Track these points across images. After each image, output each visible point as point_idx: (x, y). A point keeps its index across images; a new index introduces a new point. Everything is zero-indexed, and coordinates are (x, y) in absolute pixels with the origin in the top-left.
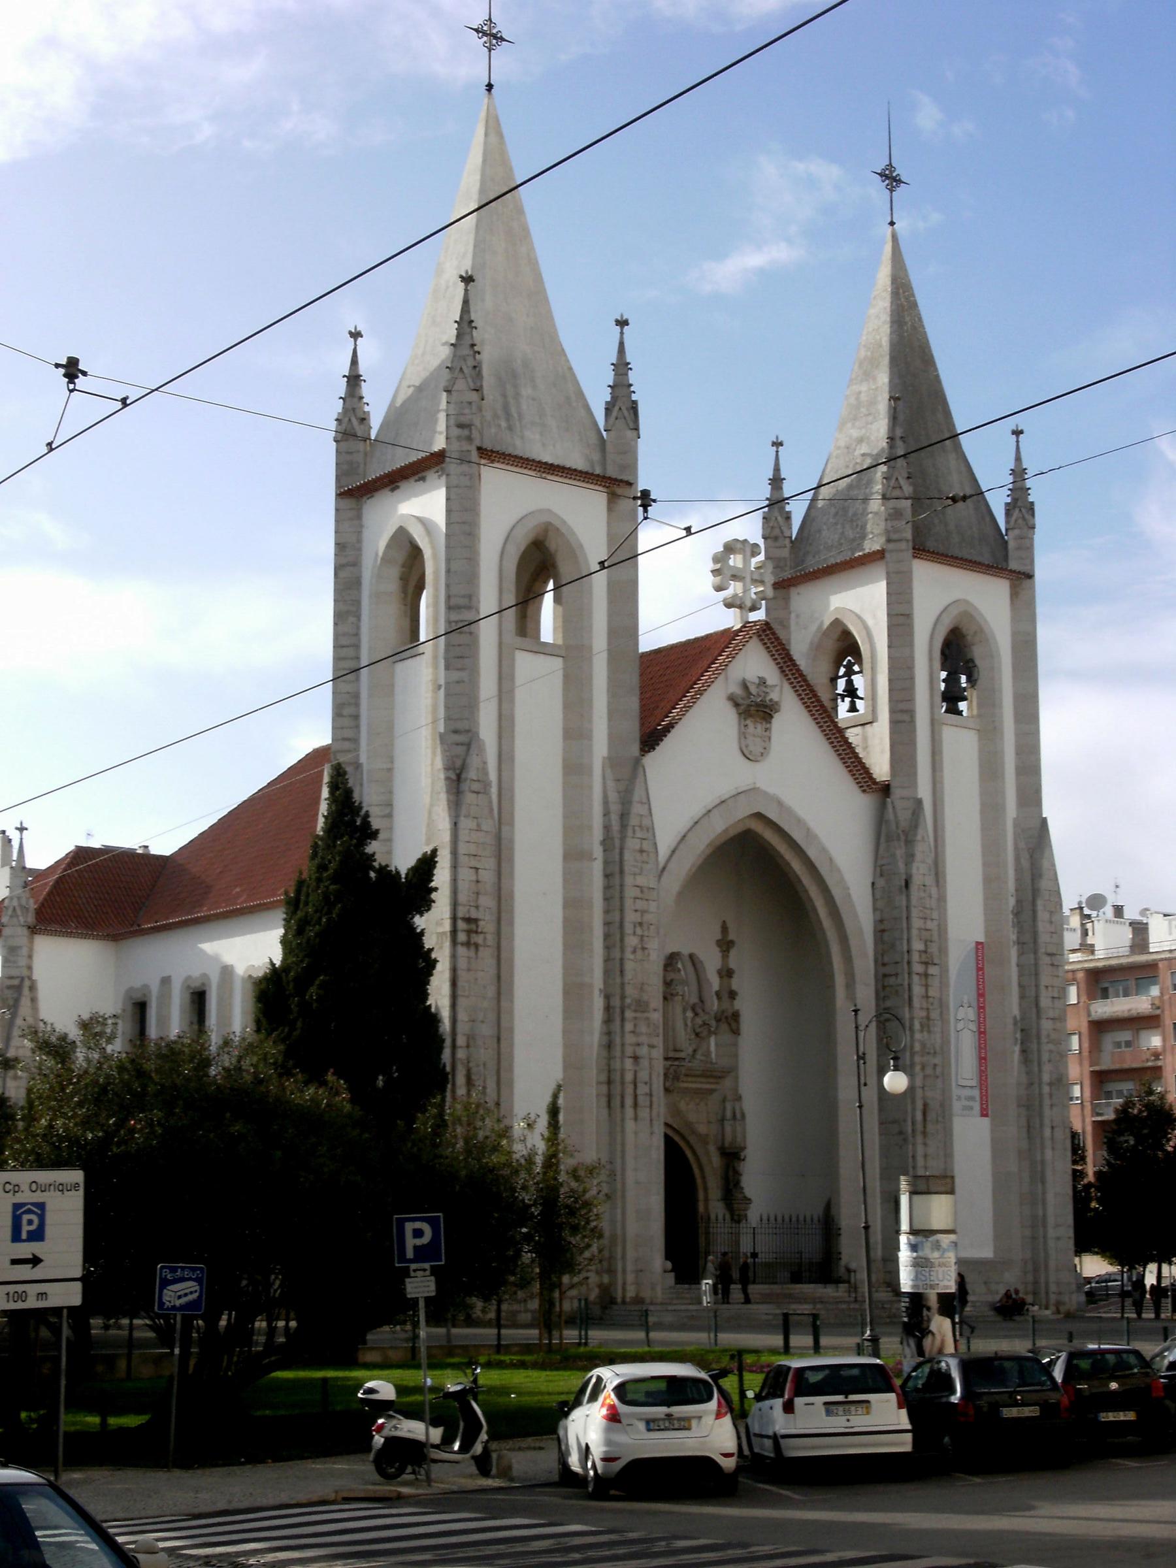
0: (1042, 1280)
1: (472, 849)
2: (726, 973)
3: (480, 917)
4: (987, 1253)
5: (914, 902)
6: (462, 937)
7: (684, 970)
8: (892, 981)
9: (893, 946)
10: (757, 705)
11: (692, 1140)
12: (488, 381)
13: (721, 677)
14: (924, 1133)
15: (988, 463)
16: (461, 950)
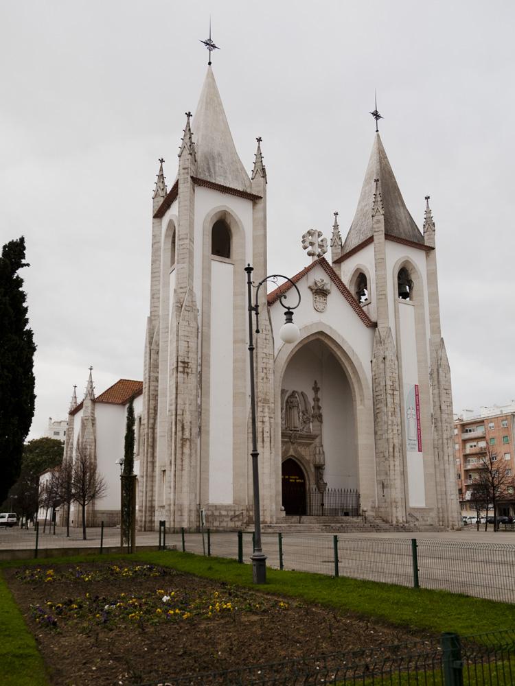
0: (446, 516)
1: (186, 334)
2: (317, 400)
3: (189, 361)
4: (423, 505)
5: (387, 366)
6: (180, 369)
7: (299, 398)
8: (379, 397)
9: (379, 384)
10: (320, 290)
11: (303, 461)
12: (199, 156)
13: (306, 276)
14: (394, 456)
15: (416, 210)
16: (179, 374)
